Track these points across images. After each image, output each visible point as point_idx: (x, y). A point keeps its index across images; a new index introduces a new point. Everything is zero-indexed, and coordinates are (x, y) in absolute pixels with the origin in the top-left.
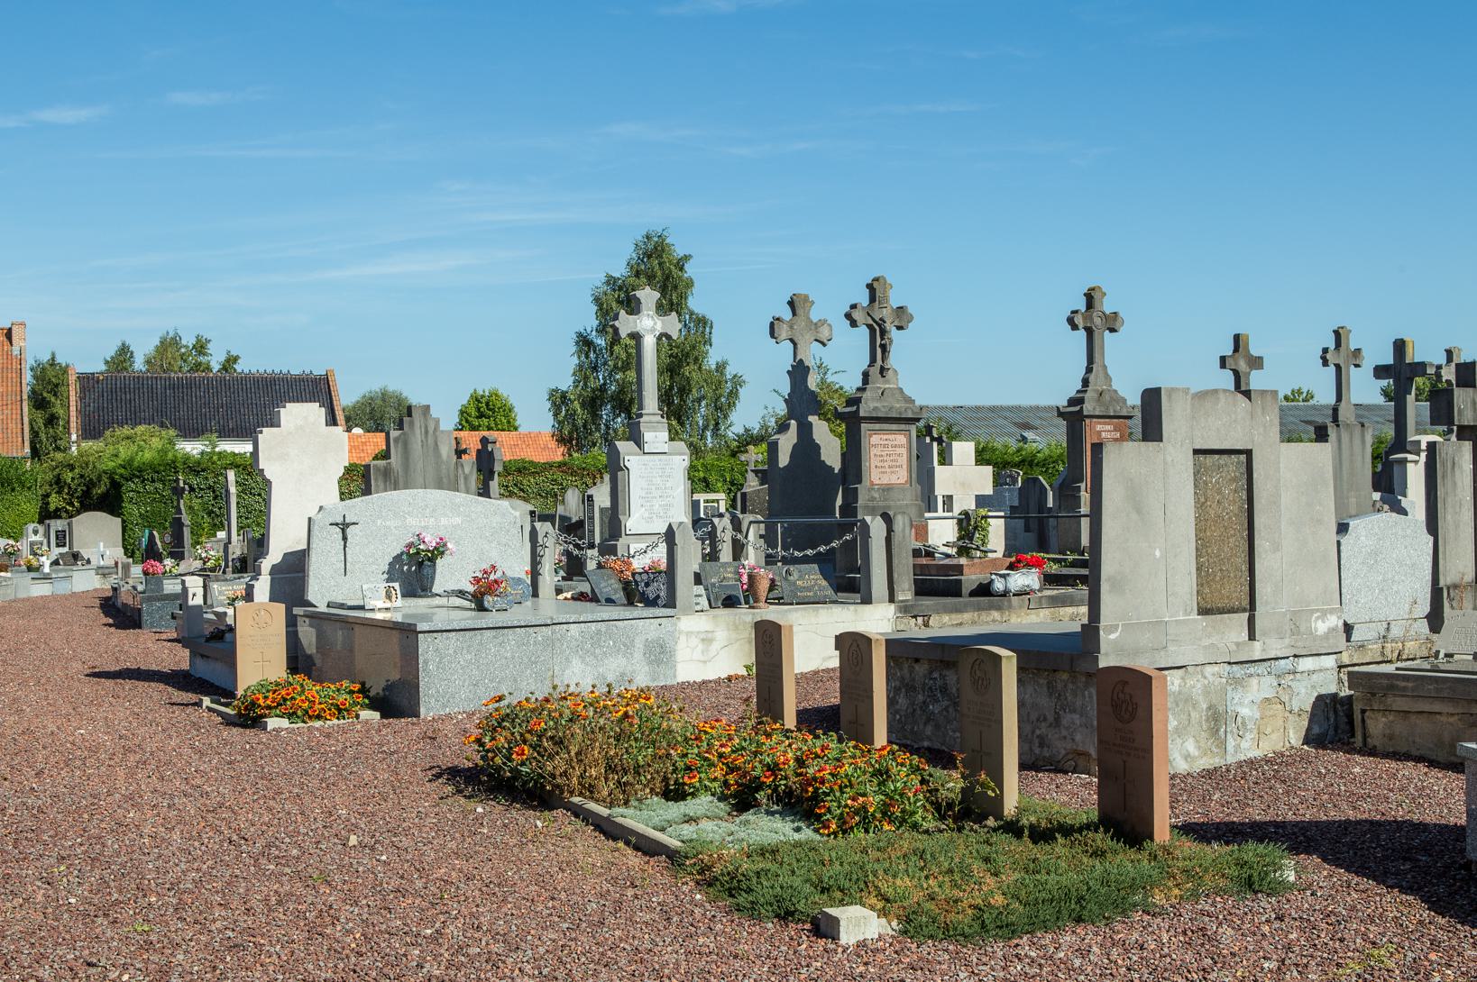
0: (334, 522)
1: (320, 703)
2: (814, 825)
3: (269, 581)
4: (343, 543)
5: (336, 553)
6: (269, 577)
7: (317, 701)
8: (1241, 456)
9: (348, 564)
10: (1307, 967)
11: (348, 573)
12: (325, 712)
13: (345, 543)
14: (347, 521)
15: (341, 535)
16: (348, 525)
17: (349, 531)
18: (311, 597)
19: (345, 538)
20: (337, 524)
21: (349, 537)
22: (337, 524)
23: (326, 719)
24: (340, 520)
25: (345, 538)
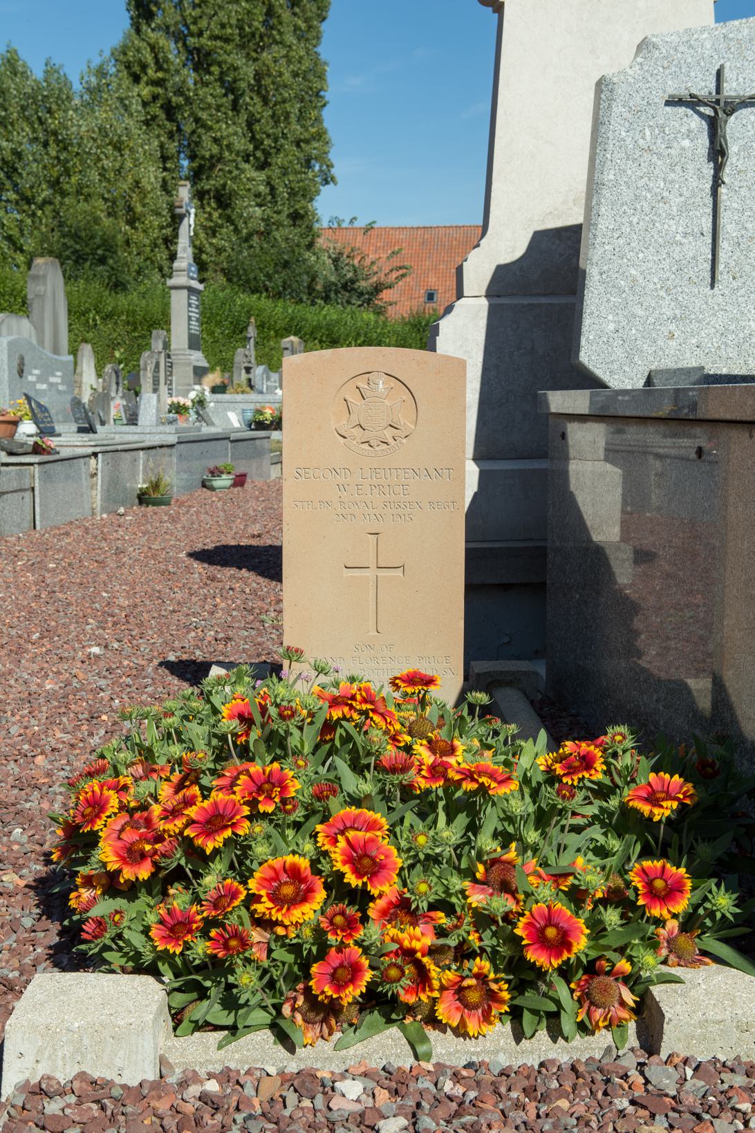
0: (683, 93)
1: (403, 909)
2: (299, 187)
3: (485, 314)
4: (708, 170)
5: (684, 208)
6: (484, 302)
7: (386, 889)
8: (617, 529)
9: (724, 245)
10: (120, 172)
11: (723, 277)
12: (423, 977)
13: (718, 169)
14: (731, 88)
15: (704, 141)
16: (731, 107)
17: (737, 127)
18: (590, 355)
19: (717, 153)
20: (692, 102)
21: (733, 149)
22: (692, 102)
23: (433, 1020)
24: (703, 86)
25: (717, 153)
